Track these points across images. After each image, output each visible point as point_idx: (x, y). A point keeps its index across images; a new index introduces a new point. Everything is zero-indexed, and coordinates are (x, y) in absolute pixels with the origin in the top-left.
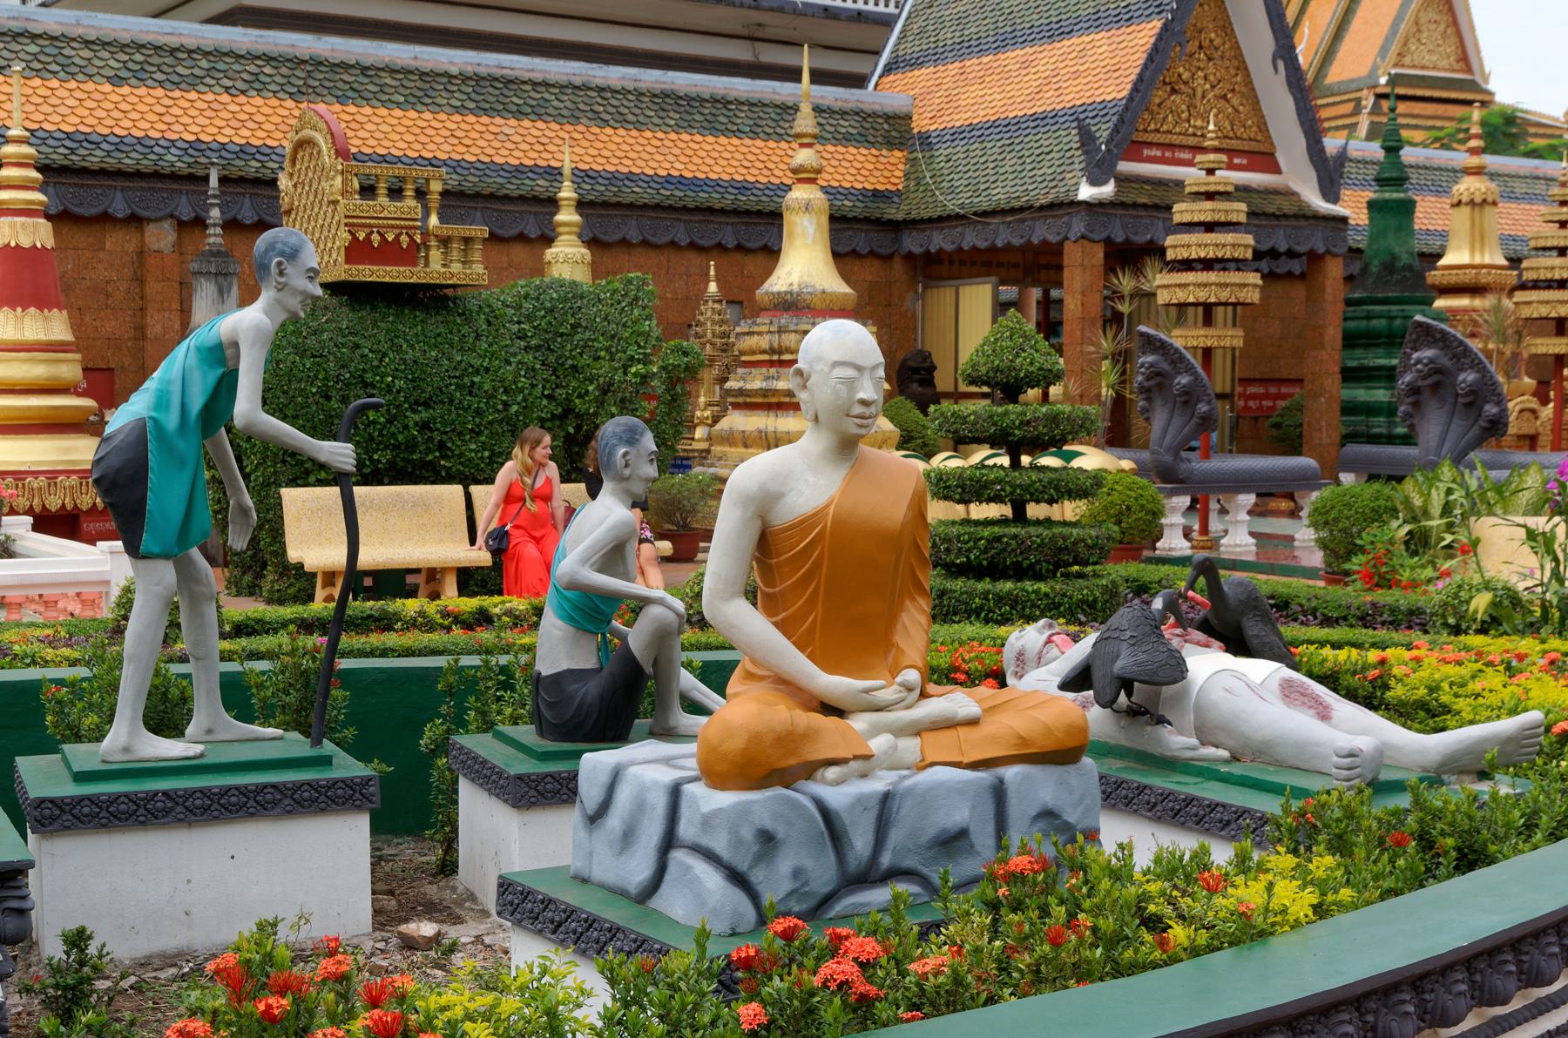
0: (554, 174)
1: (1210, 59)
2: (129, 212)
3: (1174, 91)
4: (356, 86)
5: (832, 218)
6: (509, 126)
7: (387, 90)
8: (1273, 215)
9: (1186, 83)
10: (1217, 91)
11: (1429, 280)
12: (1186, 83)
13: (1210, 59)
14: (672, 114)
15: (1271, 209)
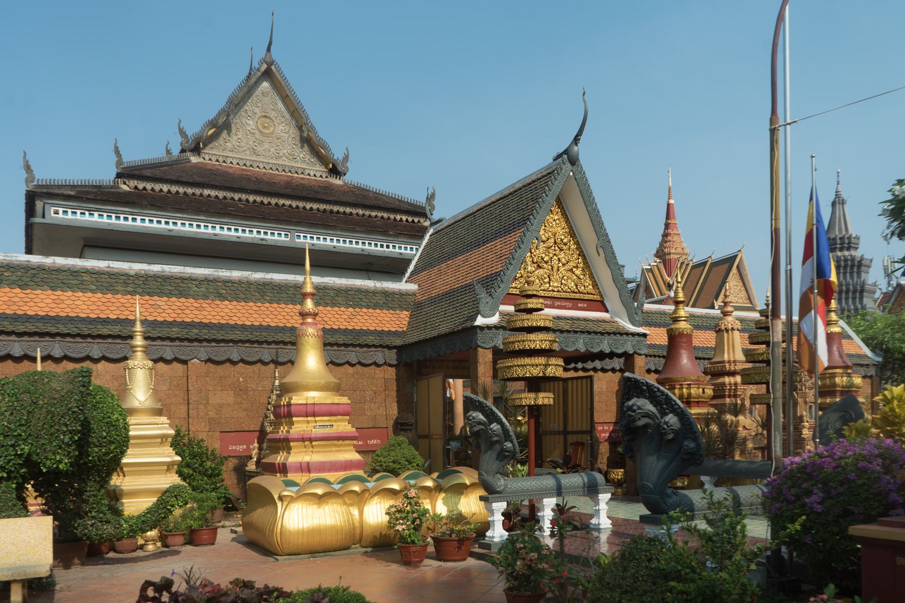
0: (132, 323)
1: (561, 250)
2: (23, 353)
3: (539, 267)
4: (65, 281)
5: (325, 345)
6: (161, 301)
7: (85, 283)
8: (600, 333)
9: (546, 262)
10: (566, 267)
11: (405, 314)
12: (546, 262)
13: (561, 250)
14: (269, 294)
15: (600, 329)
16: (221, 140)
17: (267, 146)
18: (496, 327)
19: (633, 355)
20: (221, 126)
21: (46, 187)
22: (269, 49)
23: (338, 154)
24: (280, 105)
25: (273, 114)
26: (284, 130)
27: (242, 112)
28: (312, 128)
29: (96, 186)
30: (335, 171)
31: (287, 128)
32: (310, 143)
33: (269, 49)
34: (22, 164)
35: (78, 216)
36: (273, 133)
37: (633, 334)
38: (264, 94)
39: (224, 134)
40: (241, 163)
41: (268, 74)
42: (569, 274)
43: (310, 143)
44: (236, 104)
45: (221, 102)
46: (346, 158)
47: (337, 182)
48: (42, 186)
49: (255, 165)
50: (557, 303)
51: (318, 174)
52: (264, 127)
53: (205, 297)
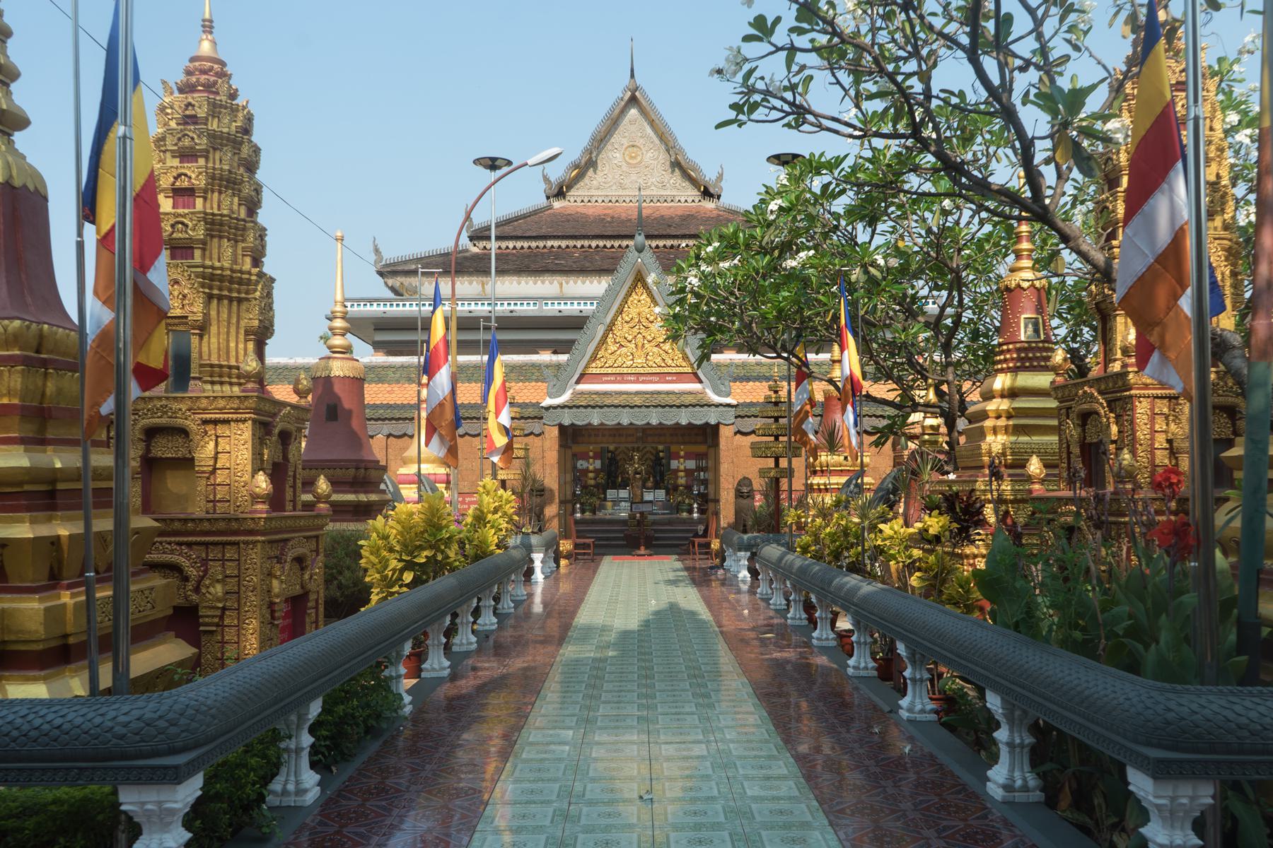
10: (654, 343)
16: (586, 180)
17: (634, 177)
18: (563, 407)
19: (718, 425)
20: (585, 166)
21: (394, 264)
22: (632, 76)
23: (709, 175)
24: (649, 130)
25: (640, 142)
26: (655, 157)
27: (609, 147)
28: (681, 150)
29: (441, 255)
30: (707, 194)
31: (656, 154)
32: (679, 166)
33: (632, 76)
34: (372, 248)
35: (362, 308)
36: (640, 162)
37: (717, 406)
38: (632, 122)
39: (590, 172)
40: (607, 200)
41: (633, 100)
42: (656, 350)
43: (679, 166)
44: (601, 140)
45: (584, 141)
46: (720, 177)
47: (709, 205)
48: (390, 265)
49: (621, 200)
50: (641, 379)
51: (690, 200)
52: (631, 158)
53: (398, 382)
